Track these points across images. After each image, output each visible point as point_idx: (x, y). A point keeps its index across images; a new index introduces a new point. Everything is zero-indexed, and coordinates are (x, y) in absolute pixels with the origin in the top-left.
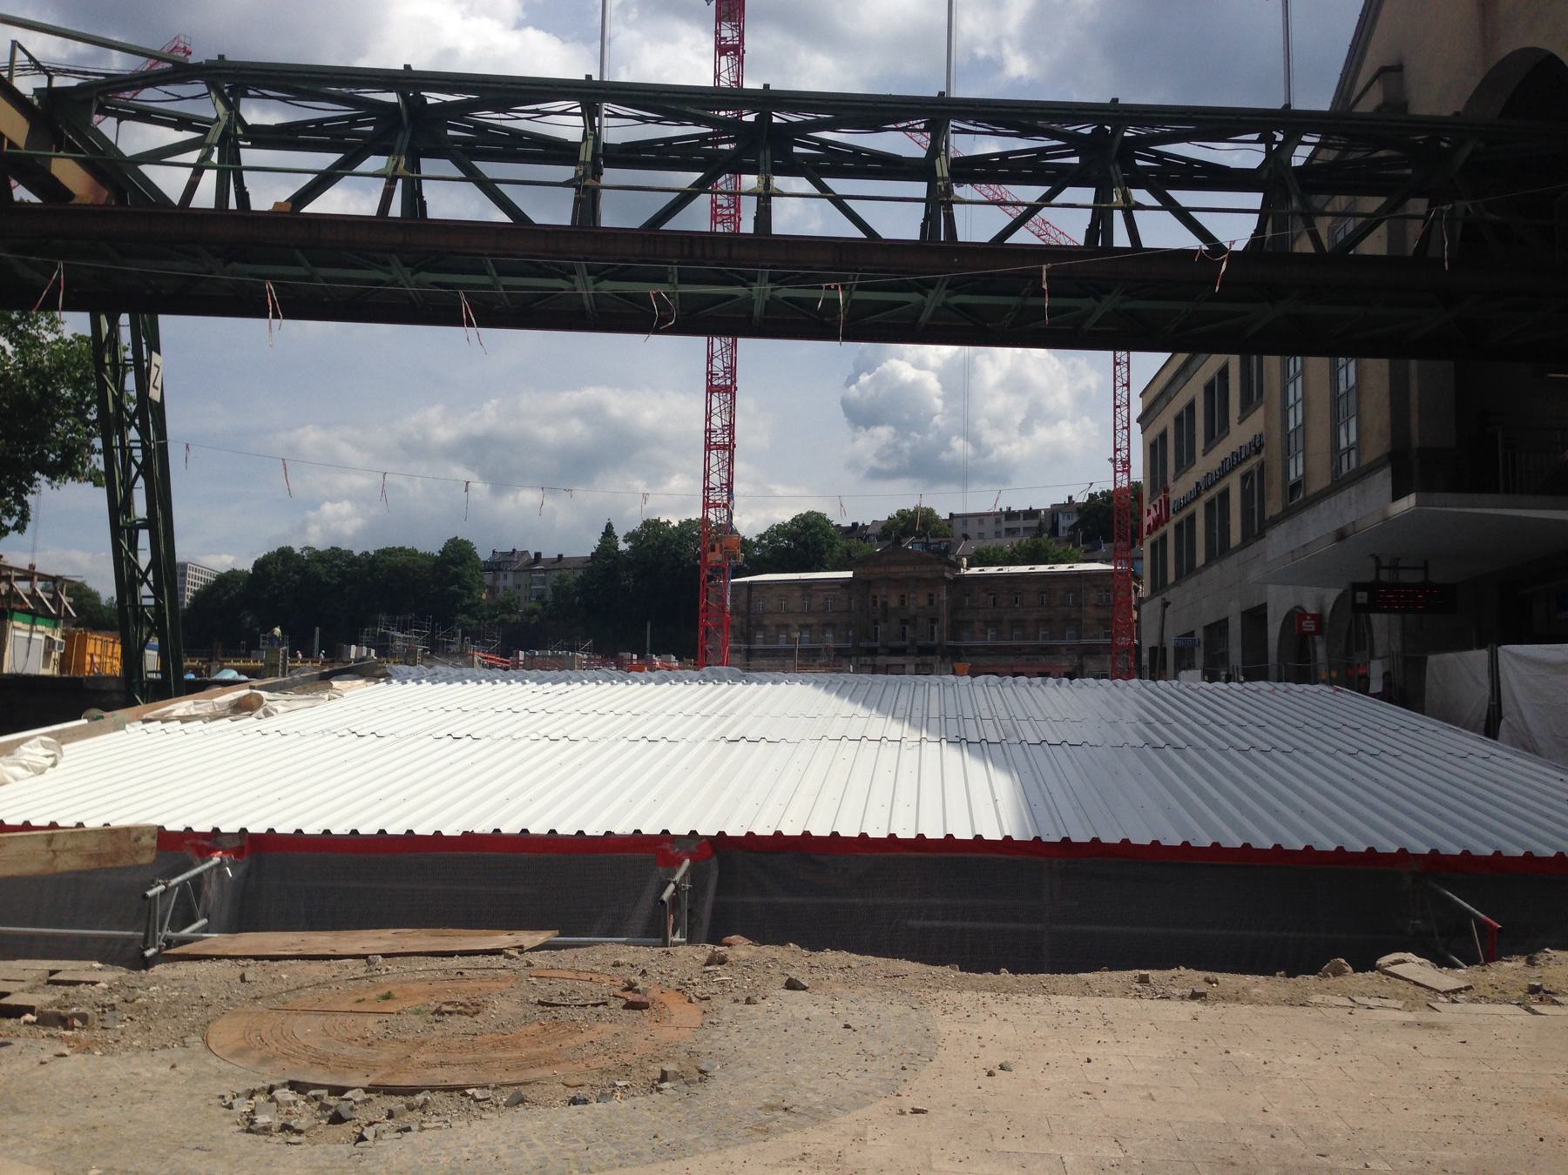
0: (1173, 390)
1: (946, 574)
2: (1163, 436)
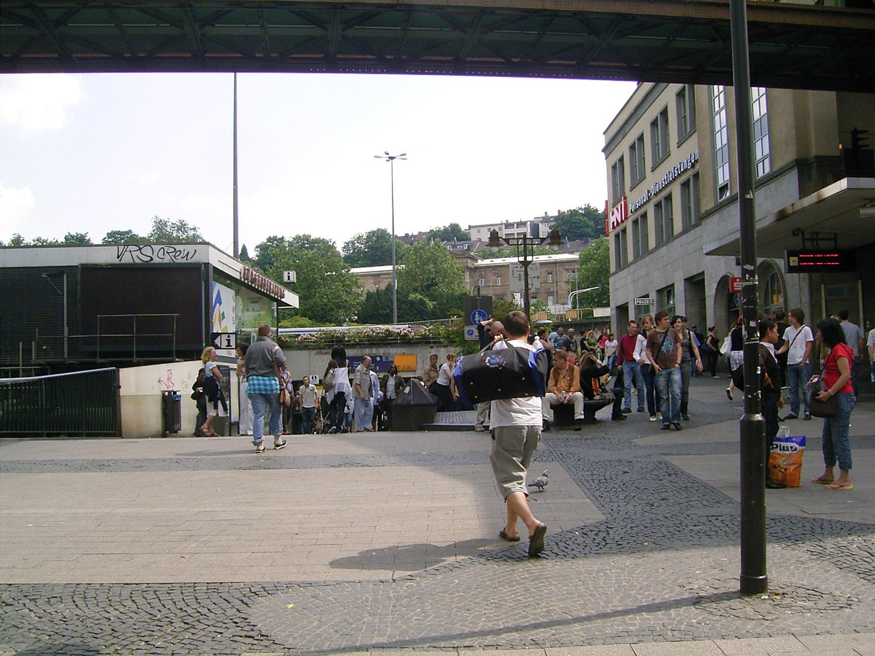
0: (627, 129)
1: (469, 265)
2: (621, 160)
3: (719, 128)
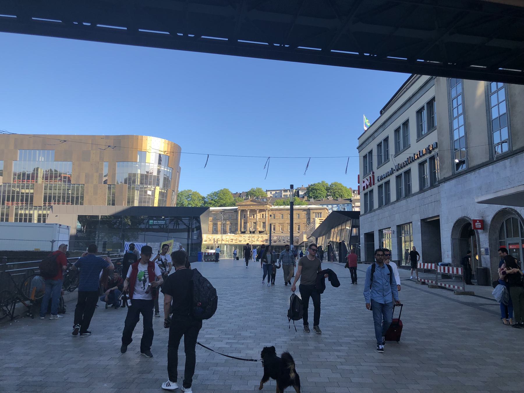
0: (386, 124)
3: (497, 103)
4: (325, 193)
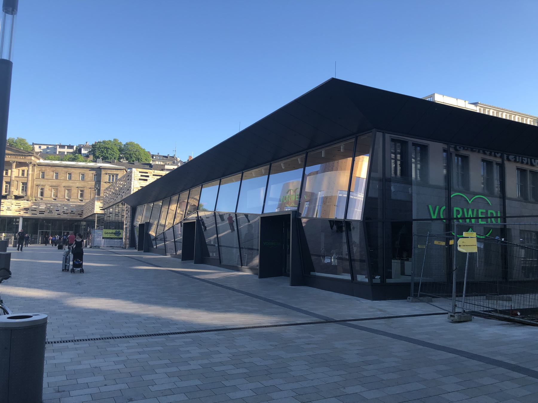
4: (117, 154)
